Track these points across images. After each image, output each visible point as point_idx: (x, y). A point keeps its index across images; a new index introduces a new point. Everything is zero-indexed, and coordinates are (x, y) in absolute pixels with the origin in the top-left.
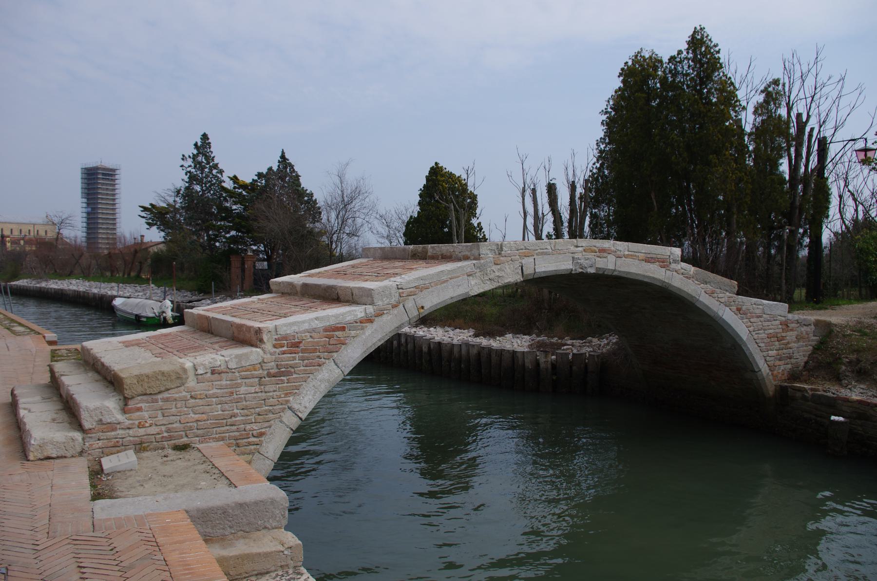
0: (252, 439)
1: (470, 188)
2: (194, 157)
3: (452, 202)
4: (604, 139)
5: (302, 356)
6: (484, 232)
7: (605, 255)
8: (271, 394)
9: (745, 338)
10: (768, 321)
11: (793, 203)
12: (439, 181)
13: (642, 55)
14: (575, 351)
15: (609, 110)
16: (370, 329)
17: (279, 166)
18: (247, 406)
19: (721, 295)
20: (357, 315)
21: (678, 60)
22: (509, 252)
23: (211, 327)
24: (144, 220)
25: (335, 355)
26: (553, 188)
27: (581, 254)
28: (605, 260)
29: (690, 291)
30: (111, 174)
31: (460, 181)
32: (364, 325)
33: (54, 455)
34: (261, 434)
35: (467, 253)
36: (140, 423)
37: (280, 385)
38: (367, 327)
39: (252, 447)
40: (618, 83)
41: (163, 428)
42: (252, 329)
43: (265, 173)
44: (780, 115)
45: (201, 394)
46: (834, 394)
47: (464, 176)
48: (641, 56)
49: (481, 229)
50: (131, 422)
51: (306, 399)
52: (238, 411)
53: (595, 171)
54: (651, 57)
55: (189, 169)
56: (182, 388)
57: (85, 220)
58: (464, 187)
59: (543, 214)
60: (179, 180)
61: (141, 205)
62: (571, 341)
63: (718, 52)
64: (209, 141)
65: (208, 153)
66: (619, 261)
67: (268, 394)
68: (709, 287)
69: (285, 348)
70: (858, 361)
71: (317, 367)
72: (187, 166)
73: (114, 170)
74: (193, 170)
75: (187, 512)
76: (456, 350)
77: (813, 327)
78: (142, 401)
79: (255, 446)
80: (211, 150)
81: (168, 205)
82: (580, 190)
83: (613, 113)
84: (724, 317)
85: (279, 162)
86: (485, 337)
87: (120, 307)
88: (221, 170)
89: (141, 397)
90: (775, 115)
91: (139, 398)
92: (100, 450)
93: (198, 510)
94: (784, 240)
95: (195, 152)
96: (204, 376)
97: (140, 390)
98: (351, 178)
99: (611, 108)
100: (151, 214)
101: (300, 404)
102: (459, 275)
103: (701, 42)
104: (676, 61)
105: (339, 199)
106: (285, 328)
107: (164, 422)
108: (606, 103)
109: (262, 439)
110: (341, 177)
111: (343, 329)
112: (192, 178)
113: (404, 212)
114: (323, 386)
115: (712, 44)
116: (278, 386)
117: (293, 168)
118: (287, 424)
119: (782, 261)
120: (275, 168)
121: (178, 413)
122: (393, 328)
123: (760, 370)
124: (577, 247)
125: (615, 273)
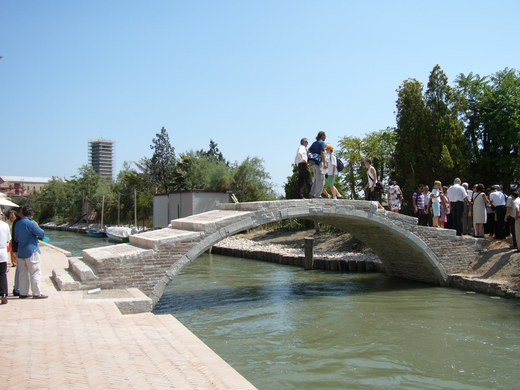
9: (424, 249)
30: (109, 146)
73: (111, 144)
75: (115, 303)
84: (409, 237)
93: (119, 302)
101: (171, 273)
106: (164, 241)
111: (190, 242)
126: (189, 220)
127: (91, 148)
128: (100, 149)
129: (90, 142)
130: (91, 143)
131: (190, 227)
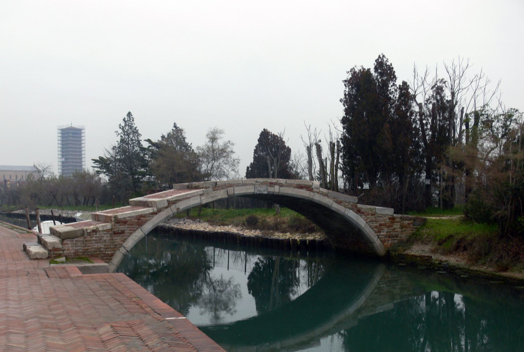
9: (363, 226)
33: (39, 258)
57: (60, 167)
60: (115, 140)
61: (93, 158)
66: (282, 188)
84: (348, 215)
123: (375, 242)
126: (145, 198)
127: (60, 135)
128: (70, 136)
129: (59, 129)
130: (60, 130)
131: (145, 204)
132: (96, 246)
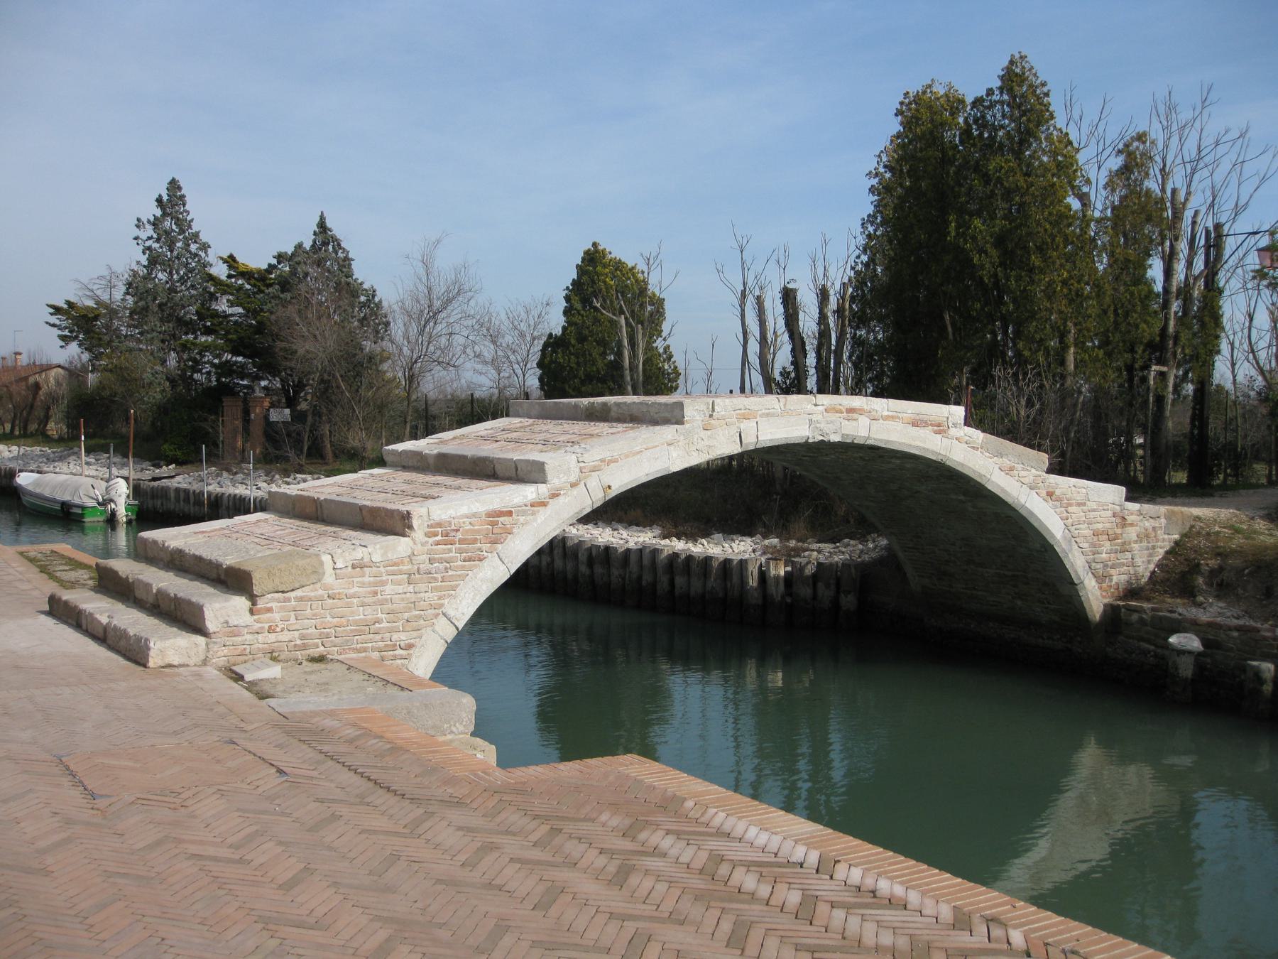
0: (399, 652)
1: (653, 287)
2: (156, 223)
3: (624, 313)
4: (875, 216)
5: (460, 549)
6: (675, 362)
7: (855, 416)
8: (422, 595)
10: (1094, 510)
11: (1164, 329)
12: (598, 274)
13: (934, 90)
14: (822, 559)
15: (882, 170)
16: (543, 514)
17: (314, 241)
18: (393, 610)
19: (1023, 473)
20: (527, 496)
21: (986, 104)
22: (723, 413)
23: (322, 513)
24: (57, 332)
25: (499, 546)
26: (791, 296)
27: (821, 416)
28: (854, 423)
29: (977, 468)
31: (634, 275)
32: (535, 509)
33: (175, 663)
34: (410, 646)
35: (668, 415)
36: (270, 627)
37: (433, 585)
38: (539, 511)
39: (399, 662)
40: (895, 126)
41: (296, 634)
42: (395, 513)
43: (290, 253)
44: (1148, 191)
45: (339, 594)
46: (1180, 614)
47: (642, 266)
48: (931, 92)
49: (670, 357)
50: (260, 625)
51: (464, 603)
52: (383, 616)
53: (859, 267)
54: (947, 95)
55: (149, 243)
56: (318, 585)
58: (642, 289)
59: (775, 332)
60: (131, 258)
61: (53, 303)
62: (818, 545)
63: (1047, 95)
64: (183, 192)
65: (182, 213)
67: (419, 595)
68: (1006, 462)
69: (439, 538)
70: (1221, 569)
71: (477, 563)
72: (145, 238)
74: (156, 245)
76: (633, 558)
77: (1163, 521)
78: (273, 600)
79: (402, 661)
80: (187, 207)
81: (98, 303)
82: (833, 304)
83: (888, 175)
84: (1027, 505)
85: (315, 233)
86: (679, 539)
87: (30, 488)
88: (204, 244)
89: (272, 595)
90: (1141, 189)
91: (269, 596)
92: (225, 658)
94: (1148, 388)
95: (159, 213)
96: (344, 570)
97: (270, 586)
98: (445, 263)
99: (885, 167)
100: (67, 319)
102: (656, 444)
103: (1021, 78)
104: (983, 106)
105: (425, 302)
107: (298, 627)
108: (876, 159)
109: (412, 652)
110: (427, 265)
112: (154, 261)
113: (524, 316)
114: (484, 587)
115: (1038, 82)
116: (430, 585)
117: (339, 245)
118: (441, 634)
119: (1147, 420)
120: (307, 245)
121: (314, 615)
122: (572, 513)
123: (1082, 583)
124: (816, 405)
125: (870, 442)
132: (360, 614)
